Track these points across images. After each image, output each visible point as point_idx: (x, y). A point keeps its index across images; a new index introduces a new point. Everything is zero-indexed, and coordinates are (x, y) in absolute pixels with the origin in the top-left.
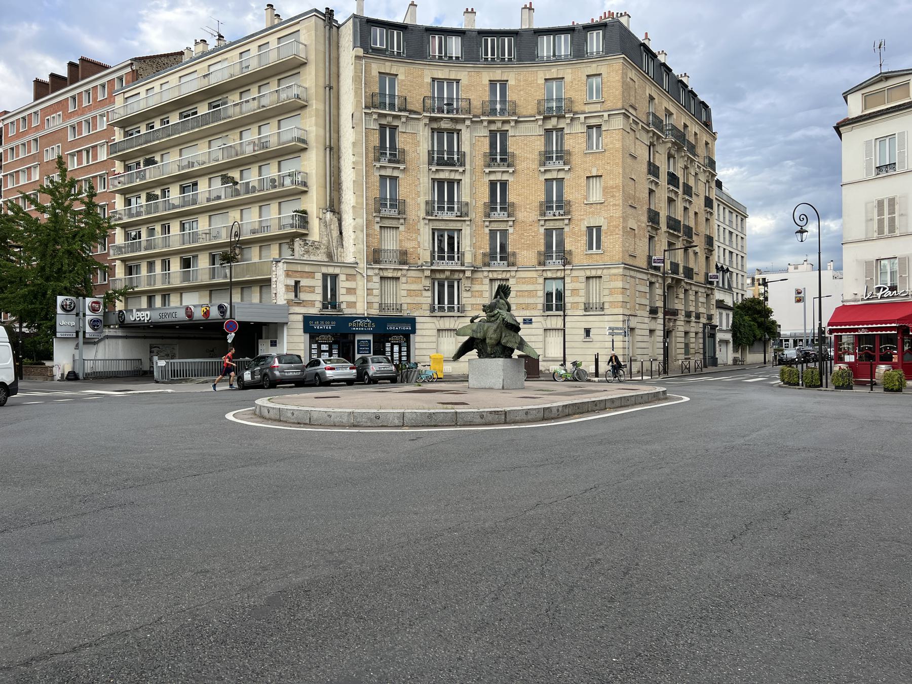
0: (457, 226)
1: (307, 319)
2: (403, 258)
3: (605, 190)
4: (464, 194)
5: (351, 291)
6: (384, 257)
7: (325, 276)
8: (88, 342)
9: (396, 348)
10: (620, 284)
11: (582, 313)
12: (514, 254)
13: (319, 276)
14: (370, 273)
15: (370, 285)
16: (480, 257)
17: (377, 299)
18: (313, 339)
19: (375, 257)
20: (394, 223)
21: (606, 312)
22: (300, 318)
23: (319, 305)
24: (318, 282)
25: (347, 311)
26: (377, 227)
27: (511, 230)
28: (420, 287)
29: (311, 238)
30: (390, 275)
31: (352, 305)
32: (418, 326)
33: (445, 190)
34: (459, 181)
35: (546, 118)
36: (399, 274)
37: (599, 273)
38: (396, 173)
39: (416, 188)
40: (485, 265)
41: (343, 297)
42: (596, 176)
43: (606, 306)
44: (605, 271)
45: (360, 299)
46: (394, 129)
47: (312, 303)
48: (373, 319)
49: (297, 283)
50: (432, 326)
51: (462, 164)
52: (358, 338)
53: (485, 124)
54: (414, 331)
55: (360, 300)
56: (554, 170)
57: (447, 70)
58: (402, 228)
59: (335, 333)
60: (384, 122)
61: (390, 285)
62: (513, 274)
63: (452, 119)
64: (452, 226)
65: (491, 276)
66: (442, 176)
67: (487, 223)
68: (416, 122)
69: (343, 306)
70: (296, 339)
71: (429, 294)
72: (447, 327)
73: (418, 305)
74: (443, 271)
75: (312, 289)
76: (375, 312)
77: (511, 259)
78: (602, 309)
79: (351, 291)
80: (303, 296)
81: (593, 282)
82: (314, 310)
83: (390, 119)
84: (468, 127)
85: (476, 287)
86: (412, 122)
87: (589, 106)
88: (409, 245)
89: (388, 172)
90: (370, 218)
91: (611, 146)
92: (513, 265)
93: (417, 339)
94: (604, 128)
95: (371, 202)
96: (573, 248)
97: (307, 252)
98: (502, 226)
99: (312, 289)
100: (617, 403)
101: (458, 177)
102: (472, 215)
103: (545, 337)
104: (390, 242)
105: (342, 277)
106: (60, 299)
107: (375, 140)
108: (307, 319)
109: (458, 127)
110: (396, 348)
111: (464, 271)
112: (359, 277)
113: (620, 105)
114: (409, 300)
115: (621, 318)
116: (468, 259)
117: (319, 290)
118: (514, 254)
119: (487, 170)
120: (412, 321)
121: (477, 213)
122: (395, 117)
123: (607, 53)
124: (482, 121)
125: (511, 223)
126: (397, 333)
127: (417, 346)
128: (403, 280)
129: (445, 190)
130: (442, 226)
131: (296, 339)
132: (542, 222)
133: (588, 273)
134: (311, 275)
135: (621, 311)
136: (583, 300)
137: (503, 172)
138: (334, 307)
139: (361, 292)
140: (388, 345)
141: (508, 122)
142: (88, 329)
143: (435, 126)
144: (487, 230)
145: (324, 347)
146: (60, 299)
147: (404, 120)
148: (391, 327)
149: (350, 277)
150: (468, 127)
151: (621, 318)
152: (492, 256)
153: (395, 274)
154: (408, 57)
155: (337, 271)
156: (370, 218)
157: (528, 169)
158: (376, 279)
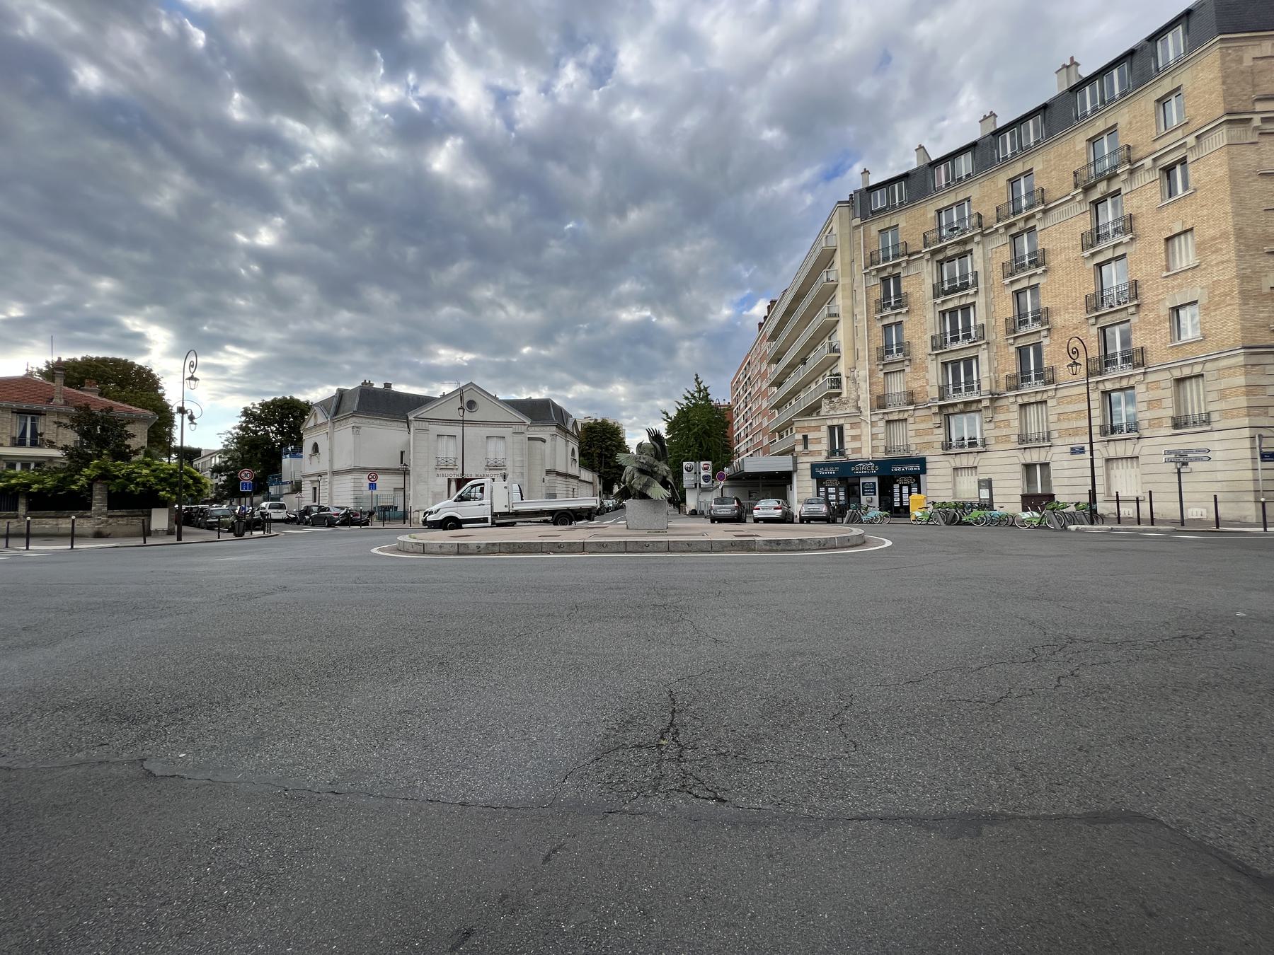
0: (972, 353)
1: (814, 467)
2: (911, 399)
3: (1200, 248)
4: (979, 317)
5: (854, 438)
6: (889, 400)
7: (831, 429)
8: (705, 490)
9: (905, 489)
10: (1241, 380)
11: (941, 451)
12: (1052, 369)
13: (824, 428)
14: (874, 418)
15: (875, 430)
16: (1003, 383)
17: (883, 443)
18: (819, 485)
19: (881, 402)
20: (899, 367)
21: (1215, 426)
22: (808, 466)
23: (825, 454)
24: (824, 434)
25: (852, 457)
26: (881, 375)
27: (1046, 341)
28: (930, 425)
29: (844, 395)
30: (1033, 400)
31: (858, 450)
32: (928, 466)
33: (956, 322)
34: (974, 304)
35: (1087, 190)
36: (906, 416)
37: (1197, 370)
38: (1034, 281)
39: (921, 325)
40: (1009, 389)
41: (848, 445)
42: (1185, 232)
43: (1214, 417)
44: (1208, 366)
45: (865, 444)
46: (897, 277)
47: (819, 453)
48: (876, 462)
49: (805, 437)
50: (947, 465)
51: (976, 284)
52: (862, 481)
53: (1002, 231)
54: (924, 471)
55: (865, 445)
56: (1107, 249)
57: (953, 194)
58: (908, 370)
59: (842, 478)
60: (885, 274)
61: (897, 428)
62: (1050, 394)
63: (957, 243)
64: (964, 355)
65: (1020, 400)
66: (950, 305)
67: (1011, 341)
68: (919, 262)
69: (848, 452)
70: (804, 484)
71: (941, 431)
72: (965, 464)
73: (929, 445)
74: (955, 404)
75: (818, 441)
76: (880, 455)
77: (1048, 376)
78: (1208, 422)
79: (854, 438)
80: (811, 447)
81: (1032, 410)
82: (821, 459)
83: (889, 270)
84: (978, 243)
85: (1000, 417)
86: (915, 264)
87: (1161, 141)
88: (915, 385)
89: (891, 320)
90: (874, 367)
91: (1207, 179)
92: (1051, 382)
93: (929, 479)
94: (1189, 160)
95: (874, 352)
96: (1147, 344)
97: (833, 408)
98: (1033, 339)
99: (818, 441)
100: (497, 549)
101: (970, 300)
102: (991, 337)
103: (1107, 469)
104: (897, 386)
105: (847, 427)
106: (685, 464)
107: (877, 293)
108: (814, 467)
109: (968, 248)
110: (905, 489)
111: (980, 401)
112: (863, 424)
113: (1220, 111)
114: (918, 440)
115: (1247, 432)
116: (986, 386)
117: (846, 439)
118: (1052, 369)
119: (1007, 281)
120: (922, 462)
121: (998, 334)
122: (894, 266)
123: (1191, 51)
124: (997, 230)
125: (1045, 333)
126: (906, 474)
127: (929, 486)
128: (911, 420)
129: (956, 322)
130: (953, 357)
131: (804, 484)
132: (1011, 341)
133: (1177, 374)
134: (818, 428)
135: (1246, 422)
136: (1171, 413)
137: (1030, 276)
138: (842, 454)
139: (866, 438)
140: (896, 487)
141: (1033, 216)
142: (703, 482)
143: (940, 257)
144: (1012, 349)
145: (831, 490)
146: (685, 464)
147: (904, 265)
148: (896, 469)
149: (853, 426)
150: (978, 243)
151: (1247, 432)
152: (1024, 376)
153: (901, 416)
154: (909, 202)
155: (841, 422)
156: (874, 367)
157: (1068, 260)
158: (882, 423)
